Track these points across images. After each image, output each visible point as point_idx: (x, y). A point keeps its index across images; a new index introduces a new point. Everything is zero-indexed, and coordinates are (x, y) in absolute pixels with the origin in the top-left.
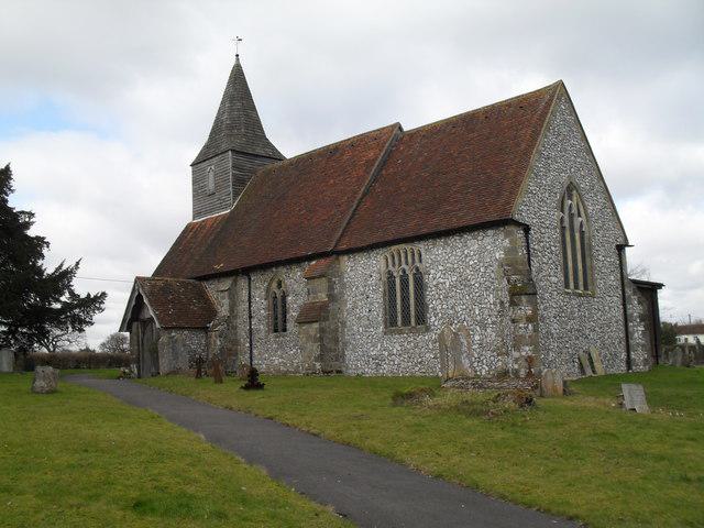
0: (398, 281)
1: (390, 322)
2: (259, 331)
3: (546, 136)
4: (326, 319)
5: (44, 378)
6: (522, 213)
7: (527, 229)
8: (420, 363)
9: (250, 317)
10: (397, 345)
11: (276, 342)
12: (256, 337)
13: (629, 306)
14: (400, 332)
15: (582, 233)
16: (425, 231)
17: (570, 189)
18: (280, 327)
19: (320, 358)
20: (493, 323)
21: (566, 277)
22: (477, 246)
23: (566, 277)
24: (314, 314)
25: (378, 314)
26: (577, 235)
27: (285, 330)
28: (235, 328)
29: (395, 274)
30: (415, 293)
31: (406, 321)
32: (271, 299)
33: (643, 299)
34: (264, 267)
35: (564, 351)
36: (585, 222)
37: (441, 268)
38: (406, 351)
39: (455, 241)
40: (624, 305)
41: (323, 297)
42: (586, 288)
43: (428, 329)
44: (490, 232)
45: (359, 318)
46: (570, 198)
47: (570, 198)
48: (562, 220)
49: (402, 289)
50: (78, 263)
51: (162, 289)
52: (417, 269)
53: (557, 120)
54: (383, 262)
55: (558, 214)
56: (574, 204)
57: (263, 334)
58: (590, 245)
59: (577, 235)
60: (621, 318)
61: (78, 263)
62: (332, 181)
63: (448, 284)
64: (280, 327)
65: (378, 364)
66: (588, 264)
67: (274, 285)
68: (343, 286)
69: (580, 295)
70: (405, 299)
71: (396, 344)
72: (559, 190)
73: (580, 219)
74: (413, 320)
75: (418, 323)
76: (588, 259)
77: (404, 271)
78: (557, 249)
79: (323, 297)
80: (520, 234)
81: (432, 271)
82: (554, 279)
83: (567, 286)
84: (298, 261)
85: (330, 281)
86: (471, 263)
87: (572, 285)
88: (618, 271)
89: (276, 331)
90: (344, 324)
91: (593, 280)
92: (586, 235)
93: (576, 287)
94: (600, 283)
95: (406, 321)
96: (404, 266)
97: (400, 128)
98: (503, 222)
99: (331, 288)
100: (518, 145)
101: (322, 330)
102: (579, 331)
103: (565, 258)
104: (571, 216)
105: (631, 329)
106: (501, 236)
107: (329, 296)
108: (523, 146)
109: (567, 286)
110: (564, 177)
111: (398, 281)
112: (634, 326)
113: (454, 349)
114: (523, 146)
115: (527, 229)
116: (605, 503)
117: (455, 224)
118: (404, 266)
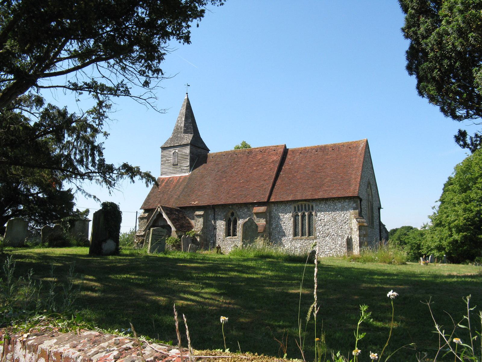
10: (299, 244)
13: (382, 234)
46: (368, 188)
88: (378, 219)
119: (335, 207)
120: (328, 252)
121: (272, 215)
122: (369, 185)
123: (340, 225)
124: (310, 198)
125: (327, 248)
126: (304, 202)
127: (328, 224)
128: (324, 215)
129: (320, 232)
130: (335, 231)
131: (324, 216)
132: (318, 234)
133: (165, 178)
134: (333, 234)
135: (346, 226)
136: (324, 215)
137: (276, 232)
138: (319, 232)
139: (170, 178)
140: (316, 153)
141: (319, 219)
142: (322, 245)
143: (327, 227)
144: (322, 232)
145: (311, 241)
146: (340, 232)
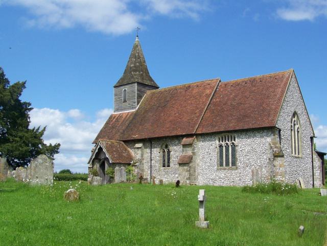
1: (221, 165)
2: (155, 166)
5: (97, 182)
6: (279, 125)
9: (151, 160)
10: (223, 175)
11: (164, 171)
12: (153, 169)
13: (314, 162)
14: (225, 169)
16: (237, 128)
17: (295, 114)
20: (265, 167)
27: (169, 166)
28: (143, 164)
31: (227, 164)
35: (291, 179)
38: (227, 177)
40: (312, 162)
43: (237, 169)
44: (265, 131)
47: (294, 118)
48: (291, 126)
50: (45, 128)
51: (110, 145)
55: (290, 124)
57: (157, 168)
61: (45, 128)
62: (190, 102)
69: (296, 157)
70: (227, 156)
71: (222, 174)
72: (291, 114)
73: (297, 126)
74: (230, 164)
83: (292, 153)
87: (294, 153)
89: (164, 166)
93: (295, 154)
95: (227, 164)
100: (276, 95)
104: (294, 125)
108: (278, 96)
113: (256, 175)
114: (278, 96)
115: (280, 130)
116: (189, 236)
117: (251, 126)
124: (232, 129)
126: (227, 134)
132: (239, 164)
133: (117, 114)
139: (121, 114)
140: (246, 85)
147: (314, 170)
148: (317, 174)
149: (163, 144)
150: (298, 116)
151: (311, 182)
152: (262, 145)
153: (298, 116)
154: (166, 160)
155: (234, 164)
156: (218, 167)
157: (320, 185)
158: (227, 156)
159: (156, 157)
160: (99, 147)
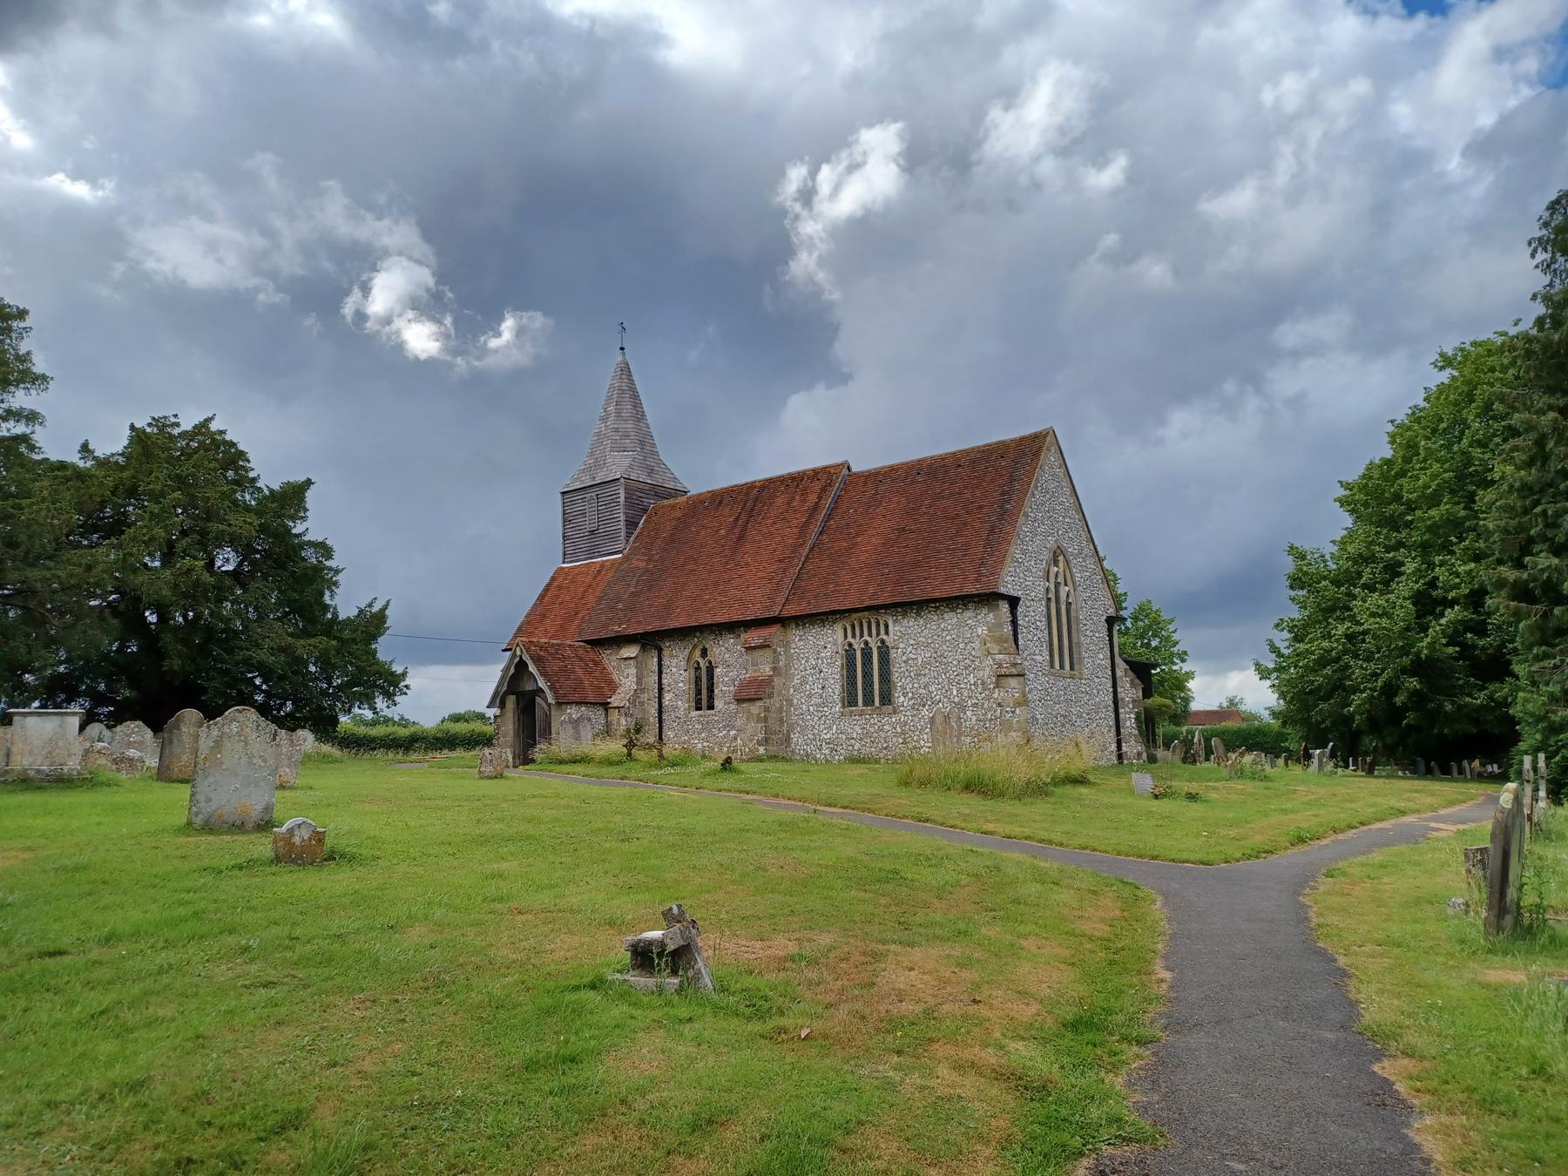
0: (859, 654)
1: (850, 700)
2: (675, 708)
3: (1033, 495)
4: (770, 696)
6: (1008, 587)
7: (1014, 602)
8: (885, 749)
9: (661, 689)
10: (857, 728)
13: (1119, 690)
15: (1069, 604)
17: (1057, 555)
18: (704, 703)
19: (766, 741)
21: (1051, 656)
22: (956, 620)
23: (1051, 656)
24: (750, 693)
25: (835, 688)
26: (1063, 608)
27: (711, 707)
29: (856, 647)
30: (880, 669)
31: (868, 701)
32: (693, 671)
33: (1138, 681)
34: (682, 633)
36: (1072, 591)
37: (912, 642)
39: (951, 619)
41: (767, 670)
42: (1072, 668)
45: (810, 696)
46: (1056, 564)
49: (863, 664)
52: (883, 642)
53: (1049, 458)
54: (840, 633)
55: (1043, 584)
56: (1061, 570)
57: (681, 713)
58: (1077, 618)
59: (1063, 608)
60: (1111, 703)
63: (920, 660)
64: (704, 703)
65: (832, 750)
66: (1075, 640)
67: (698, 653)
68: (789, 657)
70: (867, 675)
72: (1046, 555)
73: (1067, 588)
75: (883, 703)
76: (1074, 635)
77: (866, 643)
78: (1042, 624)
79: (767, 670)
80: (1004, 607)
81: (901, 645)
82: (1039, 658)
83: (1052, 666)
84: (732, 627)
85: (775, 651)
86: (948, 638)
87: (1067, 666)
89: (699, 708)
90: (790, 703)
91: (1081, 660)
92: (1073, 606)
93: (1062, 667)
94: (1088, 662)
95: (868, 701)
96: (866, 637)
97: (849, 468)
98: (989, 599)
99: (776, 660)
101: (767, 709)
102: (1065, 717)
103: (1050, 634)
104: (1057, 585)
105: (1122, 716)
106: (985, 611)
107: (774, 669)
109: (1052, 666)
110: (1051, 542)
111: (859, 654)
112: (1126, 713)
115: (1014, 602)
118: (866, 637)
119: (942, 626)
120: (927, 750)
121: (792, 651)
122: (1061, 558)
123: (955, 673)
125: (925, 736)
127: (927, 671)
128: (915, 647)
129: (907, 693)
130: (944, 691)
131: (916, 649)
132: (902, 699)
134: (938, 697)
135: (972, 675)
136: (915, 647)
137: (802, 697)
138: (905, 695)
141: (904, 658)
142: (912, 728)
143: (924, 680)
144: (910, 695)
145: (886, 719)
146: (955, 693)
147: (1121, 710)
148: (1128, 724)
149: (695, 647)
150: (1067, 562)
151: (1113, 747)
152: (961, 646)
153: (1067, 562)
154: (704, 691)
155: (886, 699)
156: (843, 706)
157: (1139, 754)
158: (867, 675)
159: (677, 683)
160: (517, 659)
